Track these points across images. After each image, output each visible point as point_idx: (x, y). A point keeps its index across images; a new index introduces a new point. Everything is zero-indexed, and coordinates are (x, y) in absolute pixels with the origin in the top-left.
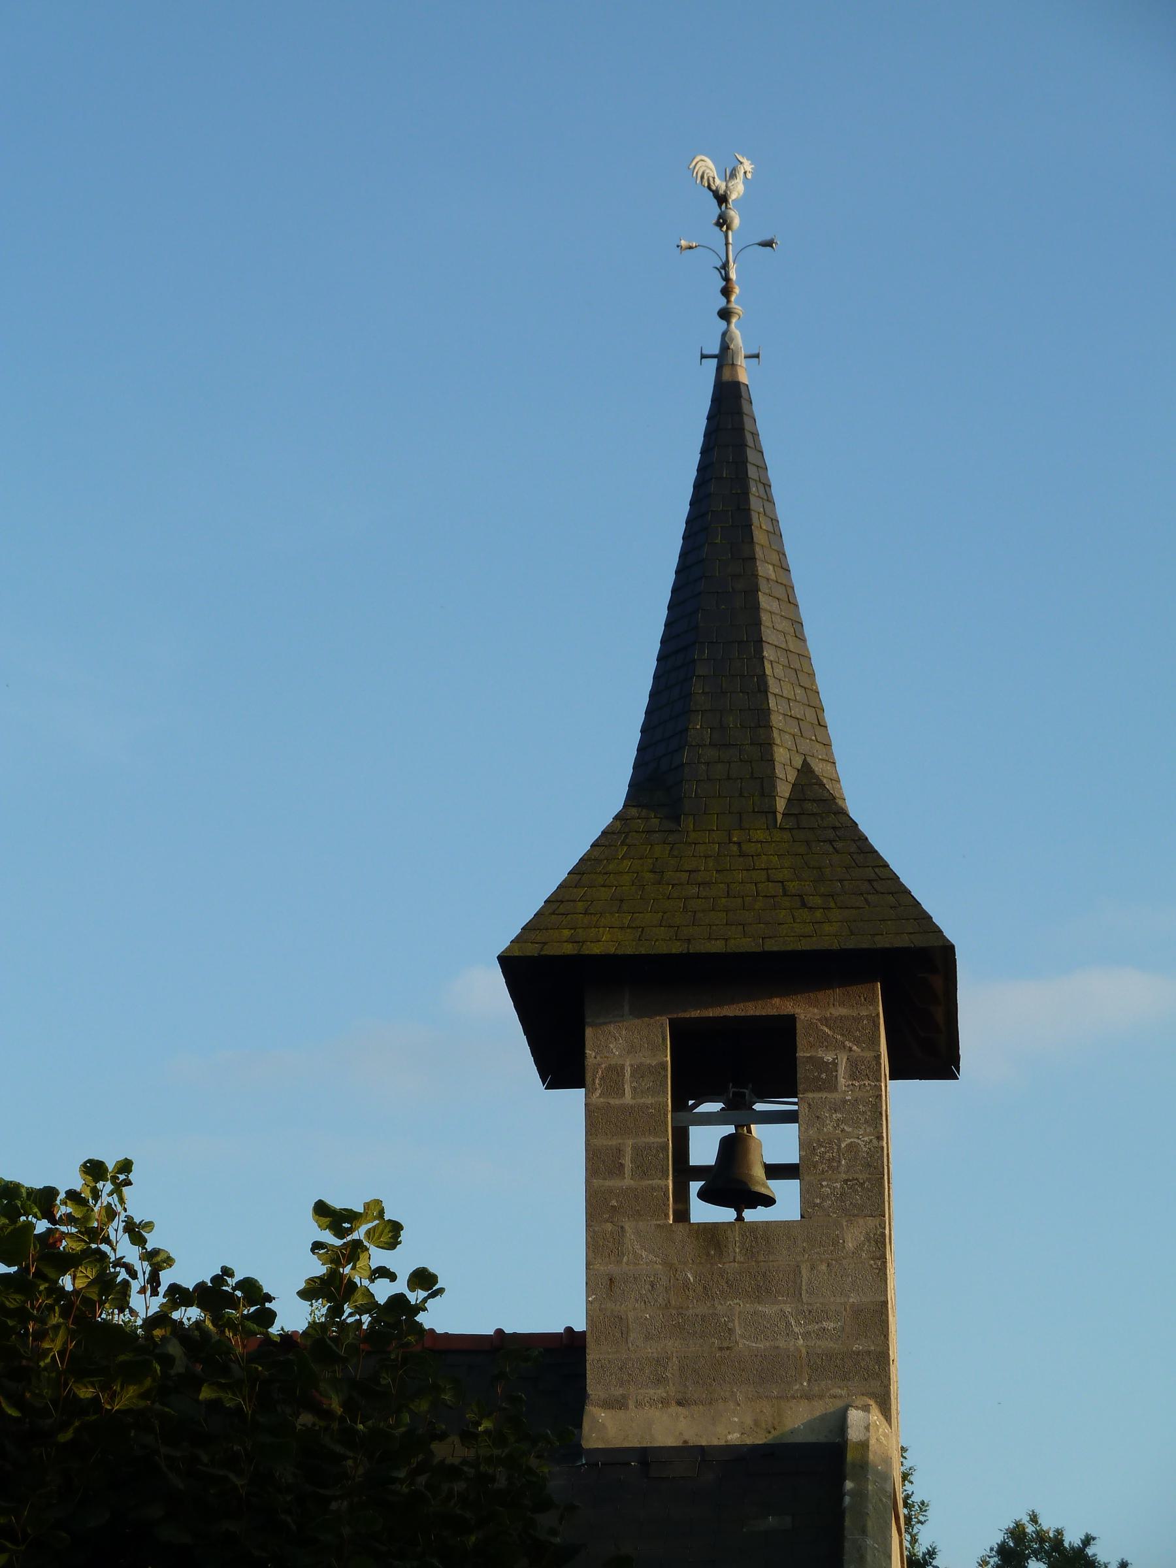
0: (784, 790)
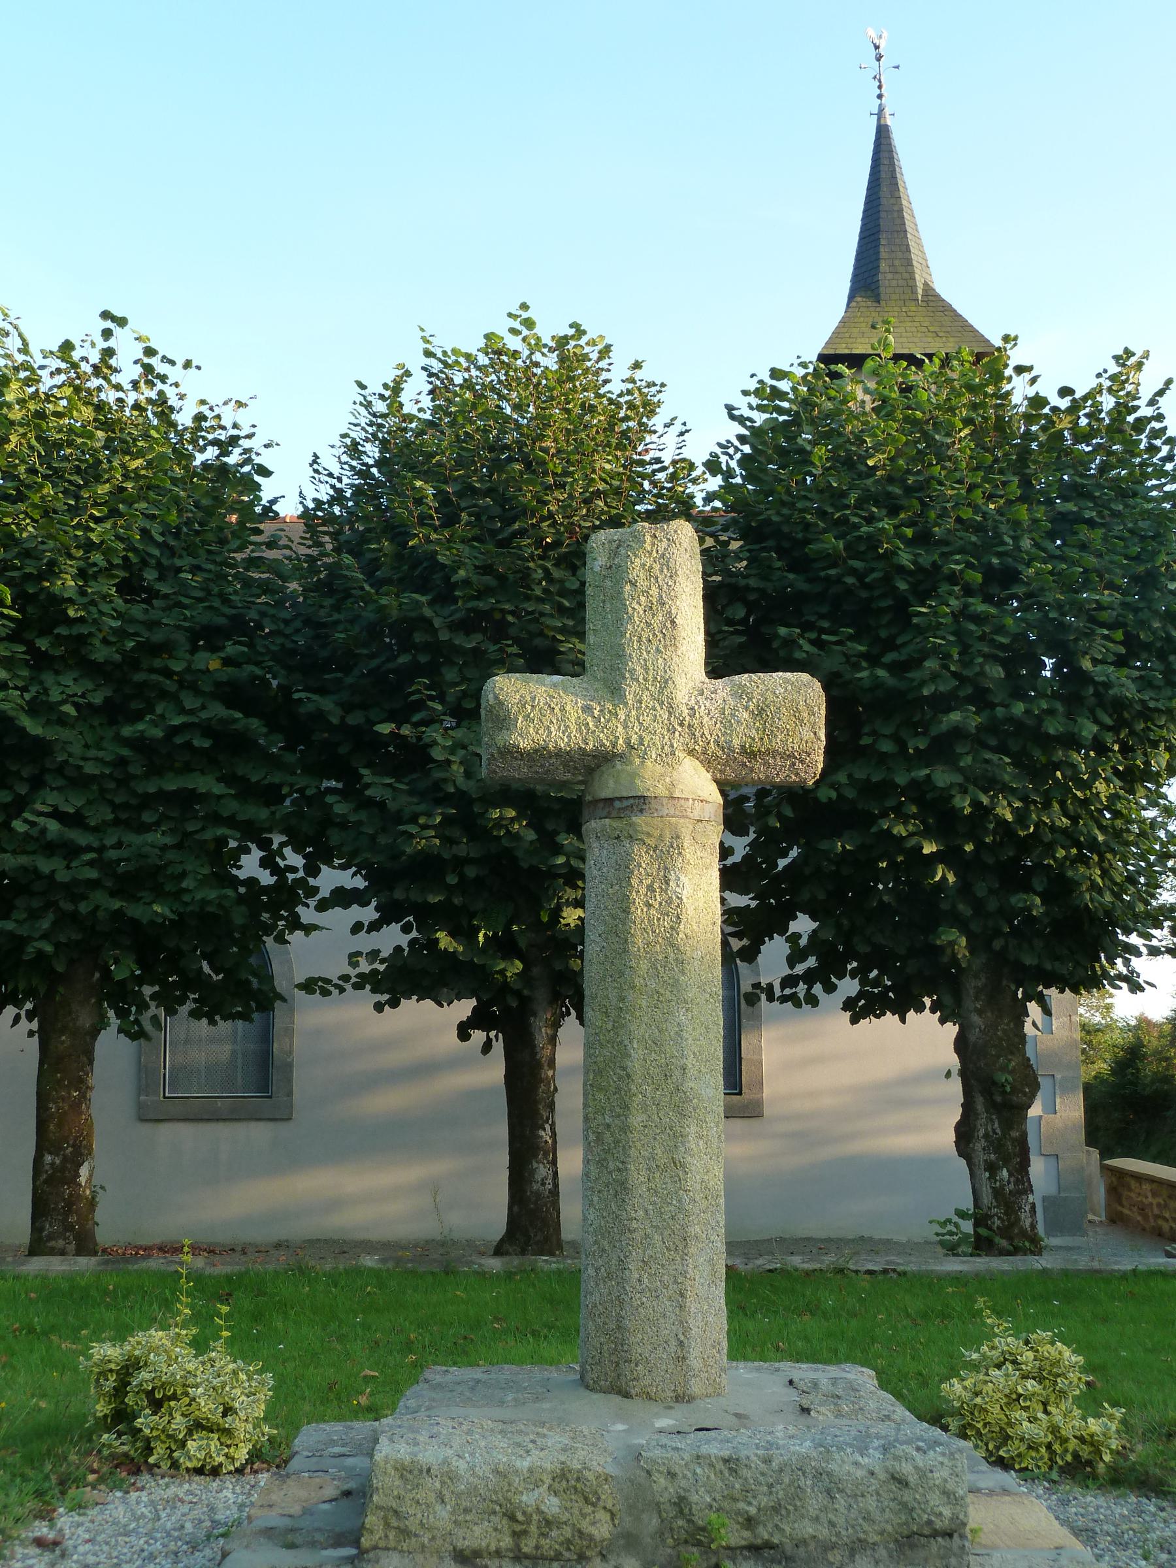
0: (920, 291)
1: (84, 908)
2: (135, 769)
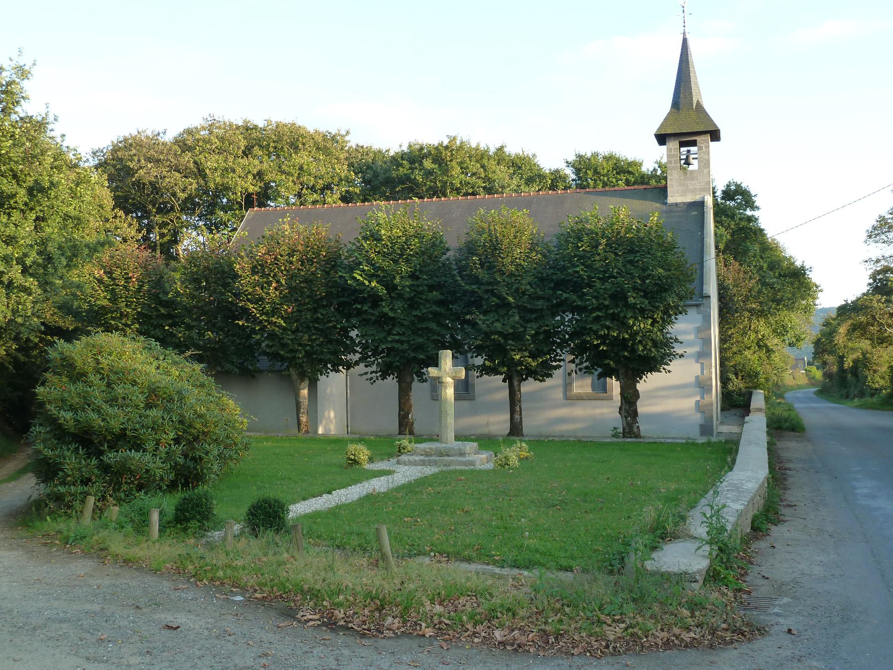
1: (406, 355)
2: (416, 322)
